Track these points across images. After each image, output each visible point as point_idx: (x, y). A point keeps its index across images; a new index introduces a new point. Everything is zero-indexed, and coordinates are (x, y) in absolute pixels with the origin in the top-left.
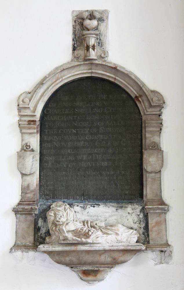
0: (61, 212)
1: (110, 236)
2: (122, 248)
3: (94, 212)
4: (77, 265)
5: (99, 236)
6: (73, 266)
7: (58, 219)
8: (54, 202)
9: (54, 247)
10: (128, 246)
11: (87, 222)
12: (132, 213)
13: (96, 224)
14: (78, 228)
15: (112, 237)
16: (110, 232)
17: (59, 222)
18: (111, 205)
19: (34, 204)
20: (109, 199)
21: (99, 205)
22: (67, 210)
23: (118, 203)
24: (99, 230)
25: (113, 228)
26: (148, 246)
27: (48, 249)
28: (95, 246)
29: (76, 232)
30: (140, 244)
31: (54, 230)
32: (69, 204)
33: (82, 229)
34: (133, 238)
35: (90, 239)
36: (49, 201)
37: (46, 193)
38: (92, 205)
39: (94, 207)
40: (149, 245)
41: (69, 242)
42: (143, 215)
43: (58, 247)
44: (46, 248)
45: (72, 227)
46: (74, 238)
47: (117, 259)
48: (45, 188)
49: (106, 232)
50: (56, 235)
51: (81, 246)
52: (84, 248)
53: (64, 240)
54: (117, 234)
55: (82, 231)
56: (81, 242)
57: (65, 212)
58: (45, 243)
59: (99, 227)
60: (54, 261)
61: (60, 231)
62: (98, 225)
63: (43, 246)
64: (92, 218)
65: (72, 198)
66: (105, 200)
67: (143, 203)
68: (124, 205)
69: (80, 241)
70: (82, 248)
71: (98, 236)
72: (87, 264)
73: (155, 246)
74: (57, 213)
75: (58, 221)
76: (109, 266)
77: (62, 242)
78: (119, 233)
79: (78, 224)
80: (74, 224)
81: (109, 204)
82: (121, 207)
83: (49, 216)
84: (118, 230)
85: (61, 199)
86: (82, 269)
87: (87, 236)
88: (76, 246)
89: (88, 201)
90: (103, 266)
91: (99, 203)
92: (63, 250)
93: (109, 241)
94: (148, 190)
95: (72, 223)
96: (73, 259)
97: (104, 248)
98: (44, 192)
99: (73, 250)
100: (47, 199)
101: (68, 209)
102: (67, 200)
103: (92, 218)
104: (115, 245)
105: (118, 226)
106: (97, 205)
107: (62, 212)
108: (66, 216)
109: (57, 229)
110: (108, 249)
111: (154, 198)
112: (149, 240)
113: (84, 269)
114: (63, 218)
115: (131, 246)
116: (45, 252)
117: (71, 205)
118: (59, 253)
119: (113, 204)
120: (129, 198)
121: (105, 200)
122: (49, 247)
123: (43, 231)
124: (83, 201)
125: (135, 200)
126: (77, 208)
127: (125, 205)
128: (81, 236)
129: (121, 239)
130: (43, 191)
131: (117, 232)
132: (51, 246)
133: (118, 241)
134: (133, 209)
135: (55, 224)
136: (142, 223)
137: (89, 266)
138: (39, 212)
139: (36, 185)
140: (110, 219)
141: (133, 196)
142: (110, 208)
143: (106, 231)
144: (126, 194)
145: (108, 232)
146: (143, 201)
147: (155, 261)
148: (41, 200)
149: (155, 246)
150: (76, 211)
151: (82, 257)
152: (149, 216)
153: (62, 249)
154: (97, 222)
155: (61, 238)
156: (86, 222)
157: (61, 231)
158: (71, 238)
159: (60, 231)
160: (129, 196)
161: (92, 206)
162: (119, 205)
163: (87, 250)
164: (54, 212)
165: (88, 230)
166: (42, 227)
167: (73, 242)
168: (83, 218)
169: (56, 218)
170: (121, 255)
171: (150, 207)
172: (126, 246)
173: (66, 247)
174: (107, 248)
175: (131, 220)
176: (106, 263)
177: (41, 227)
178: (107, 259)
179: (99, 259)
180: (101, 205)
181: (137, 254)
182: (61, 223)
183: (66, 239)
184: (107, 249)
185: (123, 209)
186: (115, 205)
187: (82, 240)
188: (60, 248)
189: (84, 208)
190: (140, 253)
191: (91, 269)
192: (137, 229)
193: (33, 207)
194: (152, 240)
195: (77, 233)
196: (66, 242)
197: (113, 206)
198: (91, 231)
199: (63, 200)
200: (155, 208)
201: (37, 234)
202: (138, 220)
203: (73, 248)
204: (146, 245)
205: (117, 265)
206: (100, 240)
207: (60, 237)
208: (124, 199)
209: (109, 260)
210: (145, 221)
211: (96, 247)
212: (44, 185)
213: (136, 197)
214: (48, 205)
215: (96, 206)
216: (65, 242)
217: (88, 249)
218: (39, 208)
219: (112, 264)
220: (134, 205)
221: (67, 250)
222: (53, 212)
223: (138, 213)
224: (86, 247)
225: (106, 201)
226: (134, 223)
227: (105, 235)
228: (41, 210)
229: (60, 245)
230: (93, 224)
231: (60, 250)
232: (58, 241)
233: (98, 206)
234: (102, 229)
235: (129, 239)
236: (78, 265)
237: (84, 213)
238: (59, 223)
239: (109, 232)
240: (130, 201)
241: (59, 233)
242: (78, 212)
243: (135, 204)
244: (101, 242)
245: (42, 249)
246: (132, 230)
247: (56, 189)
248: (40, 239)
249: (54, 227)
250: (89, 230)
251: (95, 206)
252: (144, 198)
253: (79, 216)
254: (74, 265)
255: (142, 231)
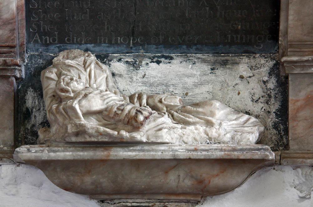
0: (73, 70)
1: (192, 127)
2: (219, 154)
3: (159, 75)
4: (113, 194)
5: (165, 125)
6: (103, 197)
7: (63, 85)
8: (63, 50)
9: (54, 151)
10: (234, 150)
11: (140, 97)
12: (250, 77)
13: (160, 101)
14: (112, 106)
15: (196, 129)
16: (192, 119)
17: (67, 91)
18: (199, 58)
19: (11, 52)
20: (196, 45)
21: (172, 58)
22: (89, 65)
23: (216, 53)
24: (167, 113)
25: (200, 110)
26: (283, 155)
27: (38, 154)
28: (153, 150)
29: (108, 116)
30: (264, 147)
31: (54, 111)
32: (98, 57)
33: (122, 108)
34: (249, 133)
35: (142, 133)
36: (52, 47)
37: (44, 29)
38: (154, 57)
39: (158, 62)
40: (288, 151)
41: (88, 139)
42: (277, 81)
43: (63, 151)
44: (35, 154)
45: (97, 104)
46: (102, 129)
47: (207, 182)
48: (42, 17)
49: (182, 119)
50: (59, 124)
51: (118, 149)
52: (125, 153)
53: (77, 134)
54: (209, 124)
55: (121, 114)
56: (119, 141)
57: (85, 70)
58: (38, 143)
59: (167, 107)
60: (55, 184)
61: (66, 113)
62: (166, 103)
63: (26, 149)
64: (154, 89)
65: (107, 42)
66: (184, 47)
67: (278, 52)
68: (230, 57)
69: (116, 138)
70: (121, 153)
71: (161, 126)
72: (137, 194)
73: (301, 155)
74: (64, 72)
75: (63, 90)
76: (189, 198)
77: (74, 139)
78: (214, 120)
79: (111, 97)
80: (102, 97)
81: (195, 56)
82: (224, 64)
83: (45, 79)
84: (212, 114)
85: (81, 44)
86: (124, 204)
87: (132, 125)
88: (107, 150)
89: (144, 49)
90: (173, 197)
91: (170, 53)
92: (76, 158)
93: (190, 140)
94: (291, 18)
95: (96, 94)
96: (101, 180)
97: (175, 155)
98: (39, 26)
99: (99, 158)
100: (47, 45)
101: (93, 66)
102: (94, 47)
103: (154, 89)
104: (203, 148)
105: (212, 105)
106: (166, 58)
107: (76, 70)
108: (87, 80)
109: (61, 107)
110: (185, 158)
111: (305, 38)
112: (288, 141)
113: (129, 204)
114: (75, 83)
115: (241, 150)
116: (31, 163)
117: (103, 58)
118: (66, 165)
119: (205, 56)
120: (244, 40)
121: (184, 47)
122: (43, 151)
123: (37, 119)
124: (131, 48)
125: (257, 46)
126: (119, 67)
127: (233, 58)
128: (120, 125)
129: (219, 135)
130: (35, 24)
131: (210, 118)
132: (47, 148)
133: (210, 139)
134: (252, 67)
135: (57, 98)
136: (273, 101)
137: (142, 199)
138: (26, 74)
139: (18, 8)
140: (197, 91)
141: (253, 36)
142: (197, 64)
143: (184, 115)
144: (236, 32)
145: (187, 119)
146: (278, 48)
147: (301, 192)
148: (31, 45)
149: (301, 155)
150: (116, 72)
151: (123, 176)
152: (290, 83)
153: (72, 155)
154: (163, 97)
155: (70, 129)
156: (137, 95)
157: (70, 112)
158: (93, 128)
159: (66, 113)
160: (244, 36)
161: (155, 60)
162: (220, 58)
163: (135, 158)
164: (58, 70)
165: (137, 110)
166: (34, 110)
167: (100, 140)
168: (133, 89)
169: (60, 82)
170: (215, 172)
171: (295, 59)
172: (229, 151)
173: (82, 151)
174: (182, 153)
175: (245, 94)
176: (180, 191)
177: (32, 110)
178: (183, 181)
179: (163, 180)
180: (175, 57)
181: (257, 172)
182: (72, 95)
183: (81, 131)
184: (181, 157)
185: (227, 66)
186: (210, 57)
187: (122, 135)
188: (68, 153)
189: (135, 66)
190: (266, 171)
191: (147, 204)
192: (261, 116)
193: (8, 60)
194: (294, 140)
195: (110, 118)
196: (83, 140)
197: (204, 61)
198: (142, 114)
199: (84, 47)
200: (307, 61)
201: (24, 125)
202: (264, 94)
203: (100, 154)
204: (279, 153)
205: (208, 197)
206: (165, 136)
207: (66, 129)
208: (232, 43)
209: (188, 183)
210: (279, 96)
211: (156, 151)
212: (38, 9)
213: (260, 39)
214: (49, 58)
215: (163, 60)
216: (80, 139)
217: (136, 156)
218: (27, 64)
219: (195, 195)
220: (254, 57)
221: (86, 158)
222: (55, 70)
223: (265, 76)
224: (130, 151)
225: (187, 47)
226: (253, 100)
227: (180, 126)
228: (32, 69)
229: (70, 147)
230: (154, 102)
231: (69, 158)
232: (64, 138)
233: (167, 61)
234: (173, 112)
235: (238, 137)
236: (116, 194)
237: (135, 78)
238: (68, 94)
239: (189, 118)
240: (246, 48)
241: (65, 119)
242: (121, 76)
243: (258, 55)
244: (167, 141)
245: (24, 154)
246: (247, 116)
247: (67, 18)
248: (29, 137)
249: (56, 105)
250: (138, 112)
251: (161, 62)
252: (280, 38)
253: (122, 84)
254: (105, 194)
255: (272, 119)
